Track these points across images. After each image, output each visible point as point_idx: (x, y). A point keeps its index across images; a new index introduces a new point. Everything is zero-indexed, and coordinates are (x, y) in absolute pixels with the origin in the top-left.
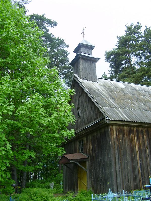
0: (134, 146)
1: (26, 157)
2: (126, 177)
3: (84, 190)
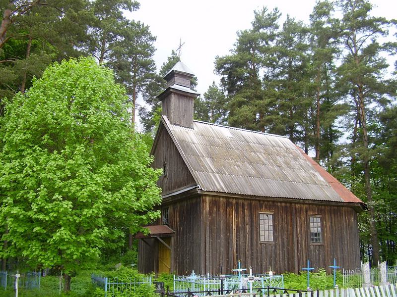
0: (231, 222)
1: (117, 236)
2: (218, 260)
3: (167, 273)
